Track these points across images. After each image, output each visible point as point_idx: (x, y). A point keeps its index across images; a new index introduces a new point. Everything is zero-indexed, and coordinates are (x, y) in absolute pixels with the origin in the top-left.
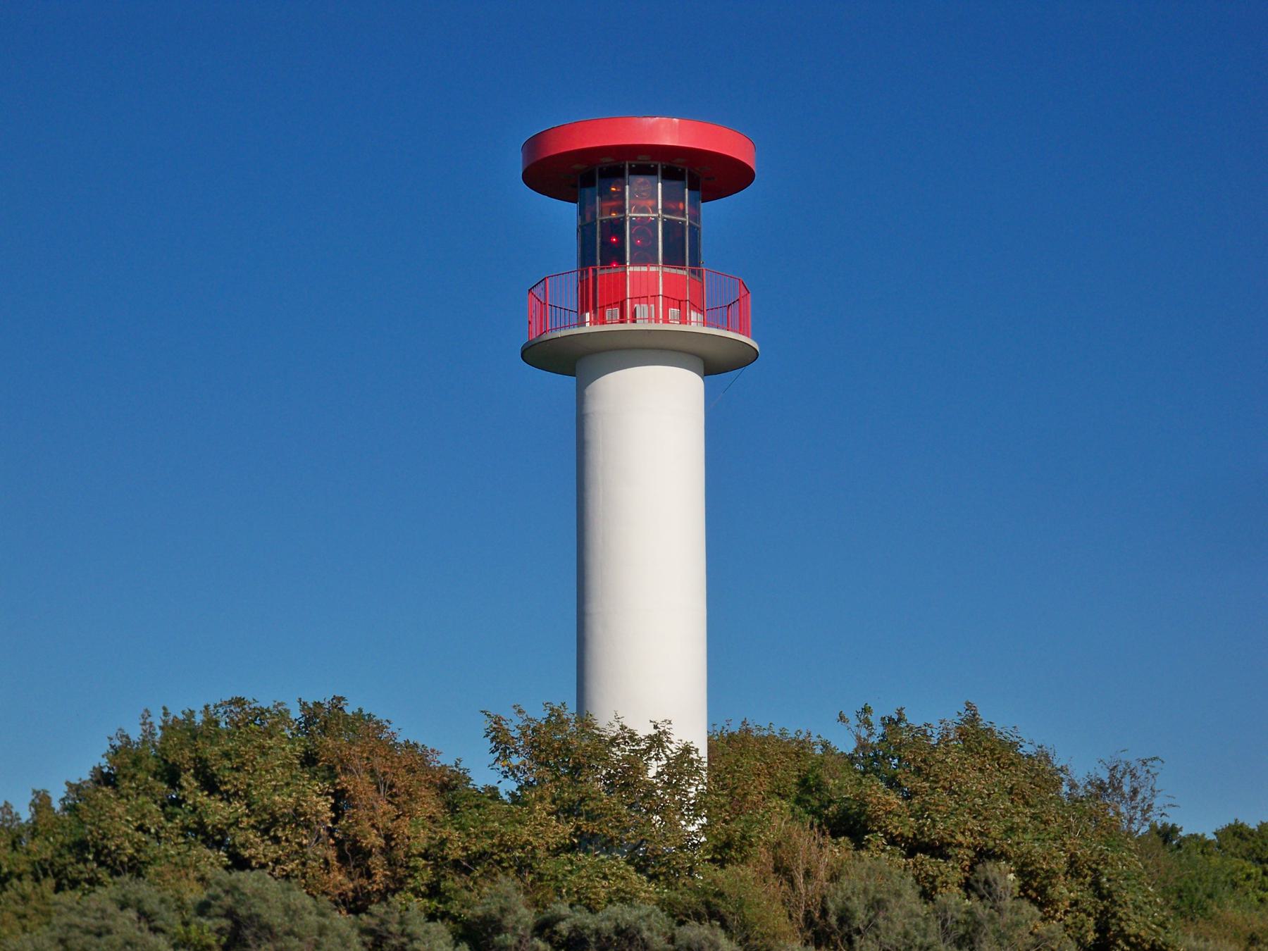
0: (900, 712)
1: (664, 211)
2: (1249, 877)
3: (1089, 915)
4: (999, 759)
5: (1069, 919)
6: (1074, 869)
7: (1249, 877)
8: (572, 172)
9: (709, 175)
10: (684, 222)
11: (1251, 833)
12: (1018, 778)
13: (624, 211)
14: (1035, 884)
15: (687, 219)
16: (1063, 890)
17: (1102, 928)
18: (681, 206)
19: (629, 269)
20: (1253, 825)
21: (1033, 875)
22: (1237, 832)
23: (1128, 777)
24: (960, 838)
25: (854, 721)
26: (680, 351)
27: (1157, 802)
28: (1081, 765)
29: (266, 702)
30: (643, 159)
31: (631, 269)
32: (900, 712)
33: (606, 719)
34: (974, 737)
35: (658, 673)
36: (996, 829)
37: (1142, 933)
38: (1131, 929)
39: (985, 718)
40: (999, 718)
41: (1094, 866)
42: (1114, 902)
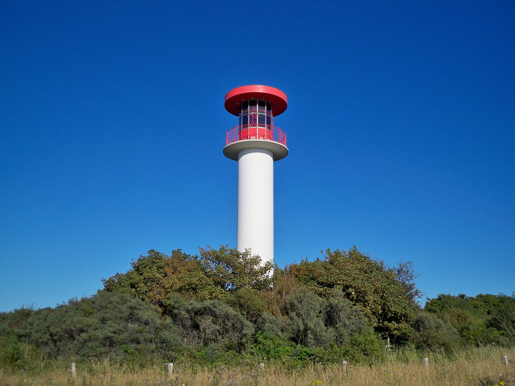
1: (259, 112)
2: (481, 305)
3: (380, 305)
5: (373, 306)
6: (376, 291)
7: (481, 305)
8: (238, 105)
9: (275, 105)
13: (247, 112)
15: (266, 114)
16: (371, 298)
17: (383, 309)
19: (249, 128)
20: (484, 294)
22: (481, 296)
23: (405, 267)
24: (339, 282)
25: (325, 252)
27: (414, 274)
28: (390, 263)
33: (242, 250)
34: (355, 256)
35: (257, 236)
36: (349, 279)
37: (397, 310)
38: (393, 309)
39: (359, 249)
40: (363, 251)
42: (386, 301)
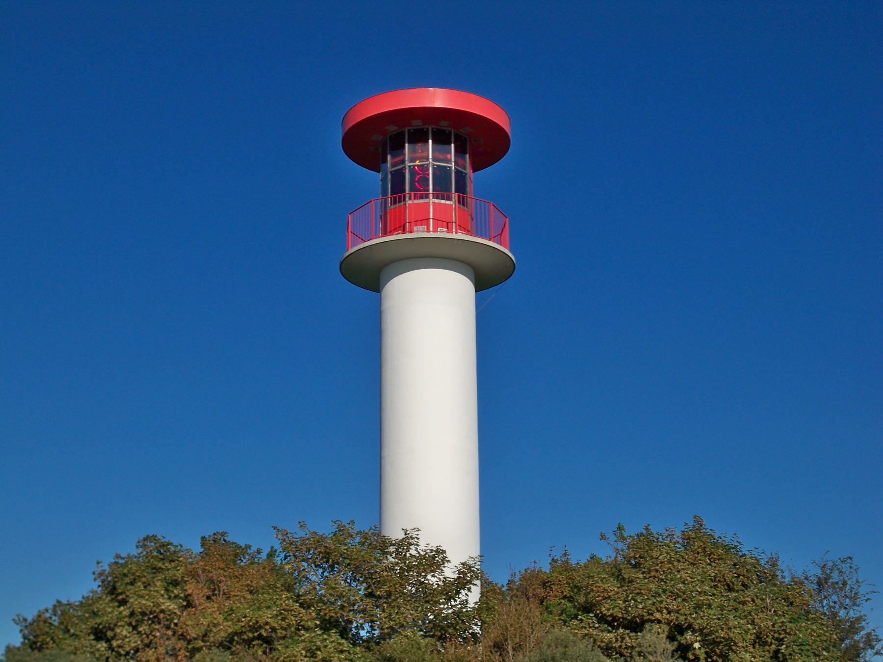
0: (647, 529)
1: (434, 159)
4: (710, 555)
8: (376, 141)
9: (479, 142)
10: (450, 168)
11: (18, 649)
12: (725, 569)
14: (718, 651)
18: (449, 156)
21: (715, 643)
24: (658, 615)
26: (453, 259)
28: (797, 564)
29: (320, 533)
30: (417, 123)
31: (410, 202)
32: (647, 529)
34: (699, 544)
40: (721, 529)
41: (776, 635)
